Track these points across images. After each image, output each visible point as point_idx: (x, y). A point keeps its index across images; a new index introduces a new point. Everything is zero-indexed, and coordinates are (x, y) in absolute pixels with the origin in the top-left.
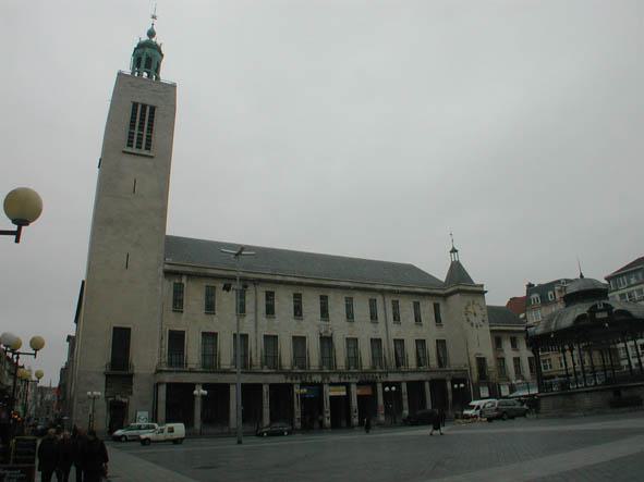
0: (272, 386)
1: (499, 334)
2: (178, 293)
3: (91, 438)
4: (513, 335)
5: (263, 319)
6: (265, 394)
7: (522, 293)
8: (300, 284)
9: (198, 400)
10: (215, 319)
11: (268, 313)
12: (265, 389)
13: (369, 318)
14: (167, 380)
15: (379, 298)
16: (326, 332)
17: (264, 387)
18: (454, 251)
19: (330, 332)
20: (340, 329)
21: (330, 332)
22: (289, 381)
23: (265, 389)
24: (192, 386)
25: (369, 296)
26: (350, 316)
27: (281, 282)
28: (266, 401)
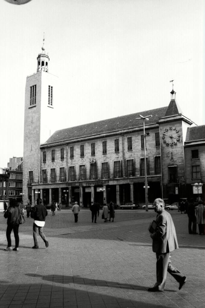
0: (52, 189)
1: (196, 148)
2: (45, 156)
3: (180, 211)
4: (193, 149)
5: (69, 160)
6: (59, 191)
7: (12, 158)
8: (82, 141)
9: (146, 191)
10: (55, 163)
11: (71, 157)
12: (118, 188)
13: (114, 151)
14: (42, 188)
15: (120, 139)
16: (93, 161)
17: (59, 189)
18: (173, 93)
19: (94, 161)
20: (100, 159)
21: (94, 161)
22: (67, 186)
23: (118, 188)
24: (68, 190)
25: (114, 138)
26: (105, 152)
27: (75, 142)
28: (118, 194)
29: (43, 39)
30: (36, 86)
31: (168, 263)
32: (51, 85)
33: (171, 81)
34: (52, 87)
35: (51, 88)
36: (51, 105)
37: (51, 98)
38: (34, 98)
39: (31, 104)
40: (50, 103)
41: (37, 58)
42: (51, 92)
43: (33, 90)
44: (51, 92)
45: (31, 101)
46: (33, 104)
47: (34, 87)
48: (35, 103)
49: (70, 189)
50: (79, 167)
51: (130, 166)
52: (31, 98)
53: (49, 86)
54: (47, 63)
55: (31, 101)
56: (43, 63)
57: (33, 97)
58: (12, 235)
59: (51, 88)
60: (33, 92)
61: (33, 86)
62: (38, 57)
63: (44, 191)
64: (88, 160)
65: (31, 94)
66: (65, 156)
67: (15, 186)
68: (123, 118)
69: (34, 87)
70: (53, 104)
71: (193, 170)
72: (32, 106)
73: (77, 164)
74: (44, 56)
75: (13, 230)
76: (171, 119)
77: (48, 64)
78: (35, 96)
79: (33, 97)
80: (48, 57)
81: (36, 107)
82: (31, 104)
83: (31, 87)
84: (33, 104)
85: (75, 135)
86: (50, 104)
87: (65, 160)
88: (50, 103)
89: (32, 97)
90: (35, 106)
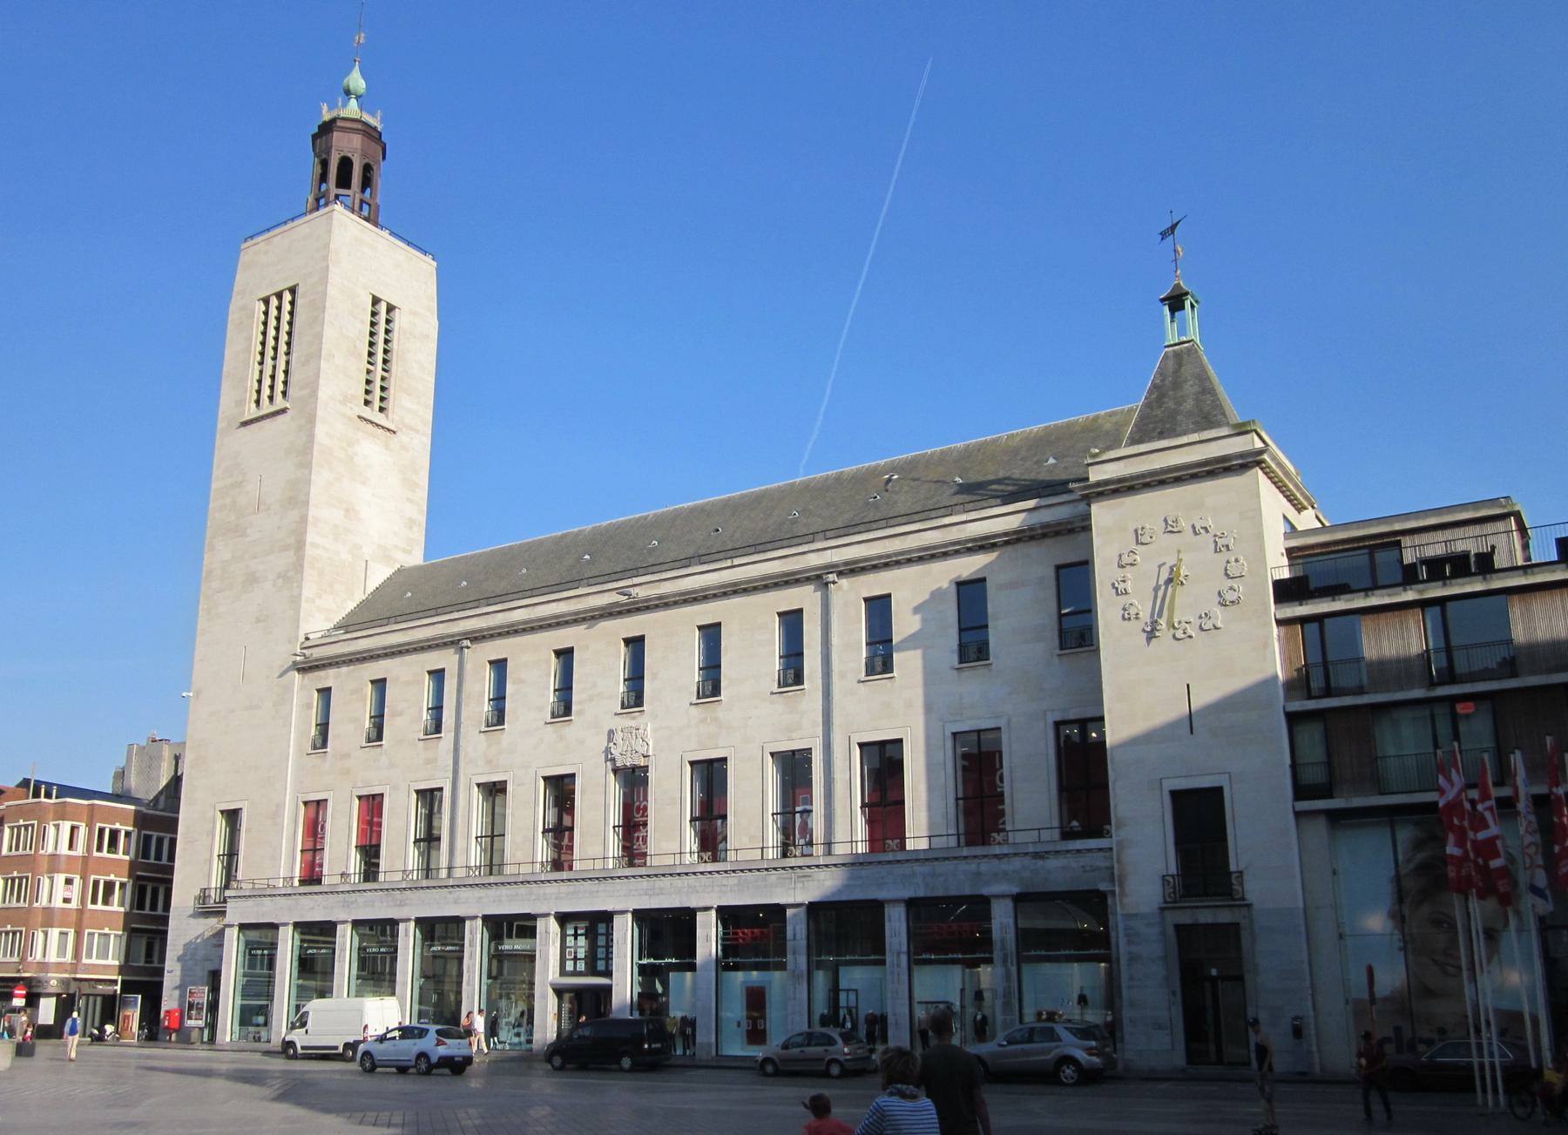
30: (293, 291)
31: (1001, 1049)
32: (387, 296)
33: (1164, 235)
34: (390, 309)
35: (383, 316)
36: (381, 409)
37: (379, 373)
41: (315, 137)
42: (381, 337)
44: (381, 337)
47: (287, 297)
51: (771, 845)
53: (376, 301)
58: (394, 1070)
59: (383, 316)
62: (316, 130)
68: (355, 614)
69: (287, 297)
70: (390, 405)
71: (1152, 1077)
72: (266, 408)
76: (922, 788)
85: (914, 475)
88: (377, 404)
90: (283, 411)
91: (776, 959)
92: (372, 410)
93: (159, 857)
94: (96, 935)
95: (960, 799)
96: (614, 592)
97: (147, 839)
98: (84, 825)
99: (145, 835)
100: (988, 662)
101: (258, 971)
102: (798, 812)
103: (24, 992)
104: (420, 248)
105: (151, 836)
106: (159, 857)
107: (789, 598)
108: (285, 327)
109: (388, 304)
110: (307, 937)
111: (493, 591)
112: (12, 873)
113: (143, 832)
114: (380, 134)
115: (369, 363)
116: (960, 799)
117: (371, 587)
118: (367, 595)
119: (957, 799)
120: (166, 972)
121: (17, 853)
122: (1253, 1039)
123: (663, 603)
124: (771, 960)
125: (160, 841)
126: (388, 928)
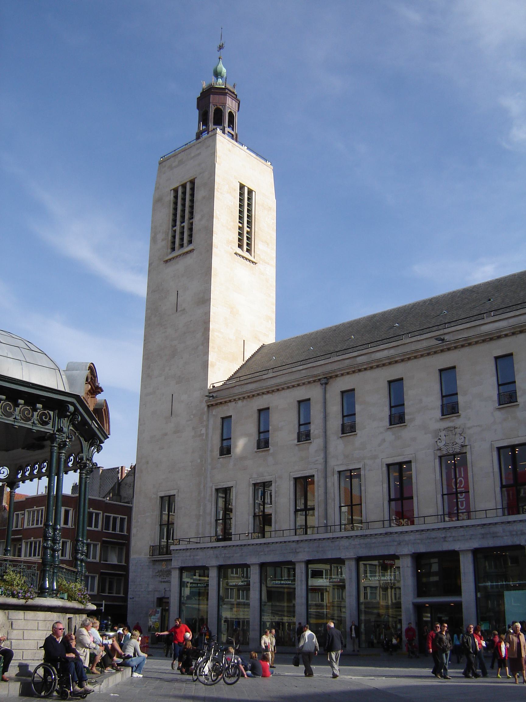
29: (218, 43)
30: (192, 182)
32: (248, 184)
34: (250, 192)
36: (248, 251)
38: (186, 224)
39: (173, 249)
40: (245, 247)
43: (183, 211)
45: (174, 237)
46: (182, 246)
48: (190, 242)
49: (174, 514)
50: (251, 489)
52: (174, 225)
53: (242, 187)
54: (231, 116)
55: (174, 237)
56: (219, 114)
57: (183, 222)
60: (184, 205)
61: (184, 186)
63: (274, 623)
64: (427, 440)
65: (175, 215)
66: (315, 429)
67: (100, 560)
73: (375, 457)
74: (223, 92)
75: (110, 648)
77: (236, 120)
78: (191, 217)
79: (183, 222)
80: (235, 97)
81: (195, 252)
82: (173, 249)
83: (176, 191)
84: (182, 246)
86: (245, 249)
87: (316, 443)
88: (245, 247)
89: (178, 223)
90: (191, 251)
91: (501, 583)
92: (243, 250)
93: (122, 530)
94: (229, 589)
95: (445, 495)
96: (433, 339)
97: (108, 518)
98: (72, 509)
99: (106, 516)
100: (230, 455)
101: (241, 600)
102: (221, 519)
103: (463, 670)
104: (262, 157)
105: (110, 516)
106: (122, 530)
107: (301, 393)
108: (187, 203)
109: (248, 188)
110: (333, 574)
111: (335, 350)
112: (31, 539)
113: (105, 514)
114: (236, 95)
115: (239, 222)
116: (445, 495)
117: (248, 356)
118: (245, 362)
119: (443, 495)
120: (129, 599)
121: (33, 527)
122: (293, 602)
123: (468, 343)
124: (499, 584)
125: (122, 520)
126: (245, 569)
